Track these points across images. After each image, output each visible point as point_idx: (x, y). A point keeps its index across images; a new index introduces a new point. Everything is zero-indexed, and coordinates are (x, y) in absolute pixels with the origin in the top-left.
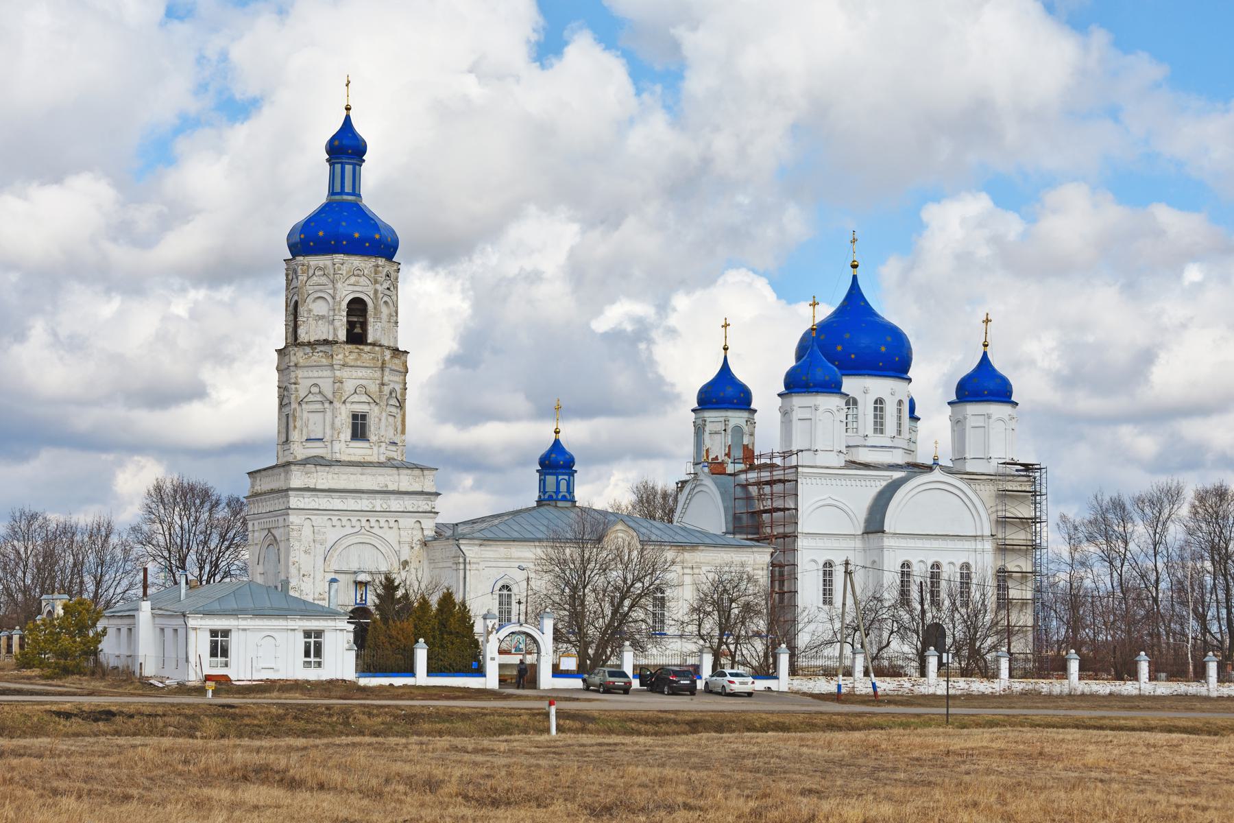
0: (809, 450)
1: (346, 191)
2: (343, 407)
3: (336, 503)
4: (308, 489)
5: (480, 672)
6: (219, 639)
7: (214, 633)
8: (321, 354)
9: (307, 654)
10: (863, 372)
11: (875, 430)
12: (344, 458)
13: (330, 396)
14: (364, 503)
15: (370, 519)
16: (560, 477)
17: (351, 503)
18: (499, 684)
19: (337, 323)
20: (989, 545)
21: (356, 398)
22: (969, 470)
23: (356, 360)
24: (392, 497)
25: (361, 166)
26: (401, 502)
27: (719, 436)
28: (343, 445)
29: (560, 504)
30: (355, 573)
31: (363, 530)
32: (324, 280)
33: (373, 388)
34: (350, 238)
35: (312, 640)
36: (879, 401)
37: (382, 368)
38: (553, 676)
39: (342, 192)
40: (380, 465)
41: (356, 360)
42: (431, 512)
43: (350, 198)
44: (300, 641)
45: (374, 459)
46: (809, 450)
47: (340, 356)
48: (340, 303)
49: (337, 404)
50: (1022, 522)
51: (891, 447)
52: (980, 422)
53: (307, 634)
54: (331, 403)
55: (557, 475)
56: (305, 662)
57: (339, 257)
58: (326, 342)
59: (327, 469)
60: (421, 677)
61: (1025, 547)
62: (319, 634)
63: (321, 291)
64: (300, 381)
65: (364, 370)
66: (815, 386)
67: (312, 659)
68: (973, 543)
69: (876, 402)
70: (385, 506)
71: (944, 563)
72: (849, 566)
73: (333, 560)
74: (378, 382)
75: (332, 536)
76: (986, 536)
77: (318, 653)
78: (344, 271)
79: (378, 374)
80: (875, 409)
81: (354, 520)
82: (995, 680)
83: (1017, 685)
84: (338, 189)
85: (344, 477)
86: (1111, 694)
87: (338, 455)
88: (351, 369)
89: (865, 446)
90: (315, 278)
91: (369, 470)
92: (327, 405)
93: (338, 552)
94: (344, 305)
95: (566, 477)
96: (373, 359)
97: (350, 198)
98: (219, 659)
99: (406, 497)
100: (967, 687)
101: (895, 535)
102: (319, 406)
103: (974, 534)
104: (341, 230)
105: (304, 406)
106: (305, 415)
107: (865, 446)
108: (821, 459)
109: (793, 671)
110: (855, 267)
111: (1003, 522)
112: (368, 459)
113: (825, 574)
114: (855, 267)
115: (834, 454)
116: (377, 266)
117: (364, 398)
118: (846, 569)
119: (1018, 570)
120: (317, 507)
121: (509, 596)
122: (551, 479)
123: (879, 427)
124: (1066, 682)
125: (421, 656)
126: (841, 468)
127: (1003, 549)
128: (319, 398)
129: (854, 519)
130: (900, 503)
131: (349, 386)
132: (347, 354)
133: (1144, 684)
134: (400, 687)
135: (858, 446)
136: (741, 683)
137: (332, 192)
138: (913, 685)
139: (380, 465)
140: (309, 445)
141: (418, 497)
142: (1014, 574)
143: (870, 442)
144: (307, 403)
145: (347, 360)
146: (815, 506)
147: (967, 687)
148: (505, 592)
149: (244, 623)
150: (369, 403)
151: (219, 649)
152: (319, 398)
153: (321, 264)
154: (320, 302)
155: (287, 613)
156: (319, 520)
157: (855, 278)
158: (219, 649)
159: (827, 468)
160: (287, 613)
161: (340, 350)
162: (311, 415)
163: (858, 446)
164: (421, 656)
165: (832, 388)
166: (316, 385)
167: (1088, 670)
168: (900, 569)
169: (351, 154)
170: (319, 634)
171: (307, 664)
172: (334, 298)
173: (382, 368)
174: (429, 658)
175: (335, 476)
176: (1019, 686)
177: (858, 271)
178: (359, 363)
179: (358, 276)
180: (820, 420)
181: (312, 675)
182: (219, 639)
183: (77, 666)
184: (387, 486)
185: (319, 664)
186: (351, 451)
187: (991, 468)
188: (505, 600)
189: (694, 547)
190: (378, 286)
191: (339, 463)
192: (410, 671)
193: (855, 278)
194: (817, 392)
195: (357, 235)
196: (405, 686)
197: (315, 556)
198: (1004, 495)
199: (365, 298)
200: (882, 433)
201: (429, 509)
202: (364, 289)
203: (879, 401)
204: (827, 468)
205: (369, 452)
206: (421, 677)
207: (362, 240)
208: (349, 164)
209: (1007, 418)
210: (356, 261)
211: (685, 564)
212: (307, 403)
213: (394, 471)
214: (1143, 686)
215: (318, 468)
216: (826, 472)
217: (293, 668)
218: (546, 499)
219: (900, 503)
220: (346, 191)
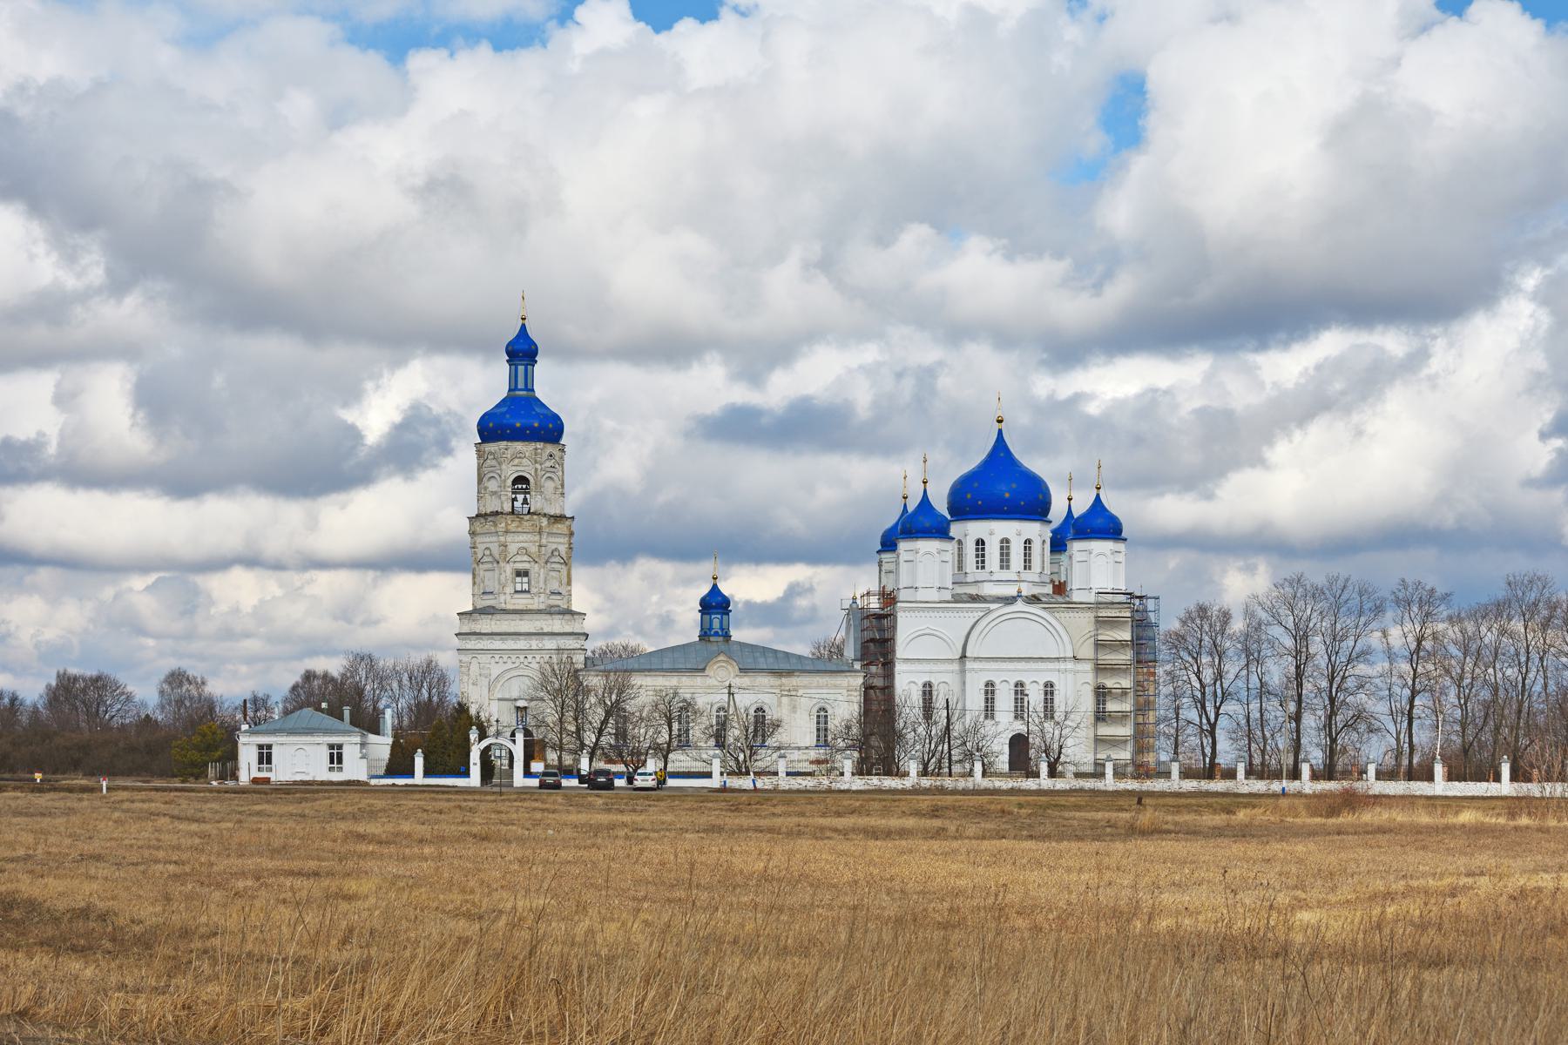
0: (912, 587)
1: (519, 387)
2: (508, 565)
3: (497, 644)
4: (475, 634)
5: (466, 774)
6: (265, 751)
7: (261, 747)
8: (491, 523)
9: (332, 762)
10: (964, 517)
11: (1002, 568)
12: (509, 607)
13: (497, 557)
14: (522, 644)
15: (536, 656)
16: (713, 616)
17: (510, 644)
18: (482, 780)
19: (503, 498)
20: (1089, 667)
21: (519, 558)
22: (1075, 600)
23: (518, 527)
24: (546, 637)
25: (534, 366)
26: (554, 642)
27: (891, 574)
28: (508, 597)
29: (712, 639)
30: (515, 700)
31: (522, 665)
32: (494, 463)
33: (533, 549)
34: (513, 428)
35: (335, 752)
36: (1028, 541)
37: (540, 533)
38: (524, 777)
39: (516, 389)
40: (539, 612)
41: (518, 527)
42: (581, 649)
43: (521, 393)
44: (325, 753)
45: (535, 607)
46: (912, 587)
47: (503, 525)
48: (505, 481)
49: (502, 564)
50: (1123, 644)
51: (1017, 581)
52: (1082, 556)
53: (331, 747)
54: (498, 562)
55: (710, 614)
56: (330, 768)
57: (503, 444)
58: (497, 513)
59: (490, 616)
60: (419, 778)
61: (1125, 667)
62: (340, 747)
63: (492, 472)
64: (478, 545)
65: (525, 535)
66: (917, 532)
67: (335, 765)
68: (1056, 663)
69: (1002, 541)
70: (540, 645)
71: (1027, 681)
72: (732, 689)
73: (497, 690)
74: (537, 544)
75: (496, 670)
76: (1069, 658)
77: (340, 761)
78: (509, 454)
79: (537, 538)
80: (1002, 548)
81: (514, 657)
82: (906, 778)
83: (925, 782)
84: (521, 385)
85: (506, 622)
86: (1012, 789)
87: (503, 605)
88: (512, 535)
89: (991, 581)
90: (488, 461)
91: (526, 616)
92: (495, 565)
93: (501, 683)
94: (509, 482)
95: (719, 616)
96: (533, 525)
97: (521, 393)
98: (265, 766)
99: (560, 637)
100: (879, 783)
101: (976, 659)
102: (490, 566)
103: (1058, 656)
104: (505, 421)
105: (481, 565)
106: (482, 573)
107: (991, 581)
108: (921, 596)
109: (984, 774)
110: (1000, 421)
111: (1099, 645)
112: (530, 607)
113: (1046, 694)
114: (1000, 421)
115: (935, 590)
116: (536, 449)
117: (526, 558)
118: (729, 691)
119: (1119, 686)
120: (482, 647)
121: (826, 717)
122: (707, 617)
123: (1005, 562)
124: (970, 779)
125: (419, 762)
126: (948, 602)
127: (1100, 669)
128: (490, 559)
129: (951, 644)
130: (982, 632)
131: (513, 548)
132: (509, 522)
133: (1440, 786)
134: (402, 786)
135: (984, 581)
136: (642, 780)
137: (510, 390)
138: (831, 783)
139: (539, 612)
140: (485, 597)
141: (568, 637)
142: (1113, 690)
143: (994, 578)
144: (482, 563)
145: (509, 527)
146: (911, 637)
147: (879, 783)
148: (822, 713)
149: (318, 739)
150: (529, 562)
151: (265, 757)
152: (490, 559)
153: (492, 450)
154: (493, 481)
155: (312, 731)
156: (484, 658)
157: (1000, 431)
158: (265, 757)
159: (927, 602)
160: (312, 731)
161: (503, 520)
162: (487, 573)
163: (984, 581)
164: (419, 762)
165: (932, 533)
166: (487, 548)
167: (1119, 774)
168: (983, 687)
169: (522, 357)
170: (340, 747)
171: (331, 769)
172: (500, 476)
173: (540, 533)
174: (425, 766)
175: (498, 622)
176: (1190, 785)
177: (526, 322)
178: (520, 529)
179: (520, 458)
180: (920, 562)
181: (336, 777)
182: (265, 751)
183: (1512, 815)
184: (542, 629)
185: (340, 769)
186: (513, 601)
187: (1092, 598)
188: (822, 720)
189: (790, 673)
190: (538, 466)
191: (505, 611)
192: (411, 774)
193: (1000, 431)
194: (917, 538)
195: (518, 425)
196: (406, 785)
197: (481, 687)
198: (1101, 622)
199: (528, 476)
200: (1030, 569)
201: (579, 647)
202: (526, 468)
203: (1028, 541)
204: (927, 602)
205: (531, 601)
206: (419, 778)
207: (523, 429)
208: (521, 365)
209: (1108, 553)
210: (519, 446)
211: (783, 688)
212: (482, 563)
213: (548, 617)
214: (1043, 782)
215: (482, 616)
216: (926, 607)
217: (319, 770)
218: (705, 635)
219: (982, 632)
220: (519, 387)
